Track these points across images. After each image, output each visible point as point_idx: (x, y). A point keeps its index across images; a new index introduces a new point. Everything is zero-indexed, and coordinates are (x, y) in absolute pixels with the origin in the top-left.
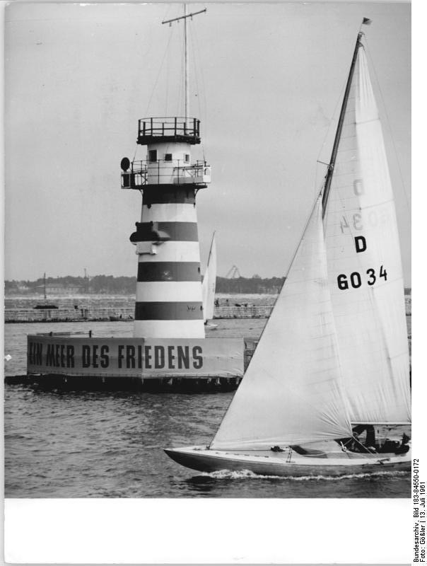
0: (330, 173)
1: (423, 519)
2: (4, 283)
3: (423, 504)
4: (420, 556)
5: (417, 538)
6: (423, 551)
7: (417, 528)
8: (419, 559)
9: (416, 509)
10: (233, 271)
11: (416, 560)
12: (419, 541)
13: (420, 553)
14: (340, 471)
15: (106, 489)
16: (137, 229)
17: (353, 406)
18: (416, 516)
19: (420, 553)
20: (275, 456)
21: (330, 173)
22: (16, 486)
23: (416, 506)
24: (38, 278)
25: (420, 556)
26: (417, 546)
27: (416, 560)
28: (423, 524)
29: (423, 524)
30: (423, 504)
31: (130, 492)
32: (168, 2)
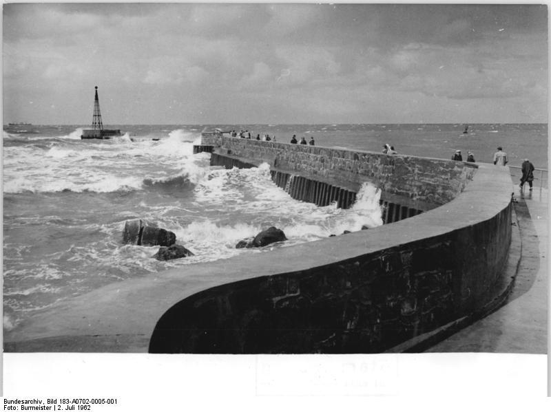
0: (97, 98)
1: (57, 408)
3: (68, 408)
4: (10, 405)
5: (27, 402)
6: (15, 408)
7: (37, 402)
8: (7, 404)
10: (30, 405)
11: (5, 401)
13: (13, 405)
14: (268, 175)
18: (49, 401)
19: (13, 405)
20: (142, 280)
21: (97, 98)
23: (58, 402)
25: (10, 405)
26: (19, 402)
27: (5, 401)
28: (52, 408)
29: (52, 408)
30: (68, 408)
31: (361, 178)
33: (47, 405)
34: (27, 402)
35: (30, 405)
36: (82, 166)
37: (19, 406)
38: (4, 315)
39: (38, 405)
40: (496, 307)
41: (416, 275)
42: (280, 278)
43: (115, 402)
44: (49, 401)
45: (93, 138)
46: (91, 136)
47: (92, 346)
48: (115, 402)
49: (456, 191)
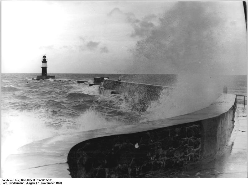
2: (41, 69)
5: (12, 181)
6: (7, 183)
7: (17, 181)
8: (3, 181)
9: (25, 180)
11: (2, 180)
12: (11, 182)
13: (6, 182)
15: (112, 93)
16: (137, 143)
17: (77, 133)
18: (22, 180)
19: (6, 182)
22: (29, 93)
23: (26, 180)
24: (234, 145)
25: (4, 182)
26: (9, 180)
27: (2, 180)
32: (1, 117)
33: (21, 182)
34: (12, 181)
35: (13, 182)
36: (60, 82)
37: (8, 182)
38: (22, 147)
39: (17, 182)
40: (147, 123)
41: (182, 139)
42: (162, 161)
43: (51, 180)
44: (22, 180)
45: (232, 148)
46: (230, 149)
47: (64, 75)
48: (51, 180)
49: (103, 94)
